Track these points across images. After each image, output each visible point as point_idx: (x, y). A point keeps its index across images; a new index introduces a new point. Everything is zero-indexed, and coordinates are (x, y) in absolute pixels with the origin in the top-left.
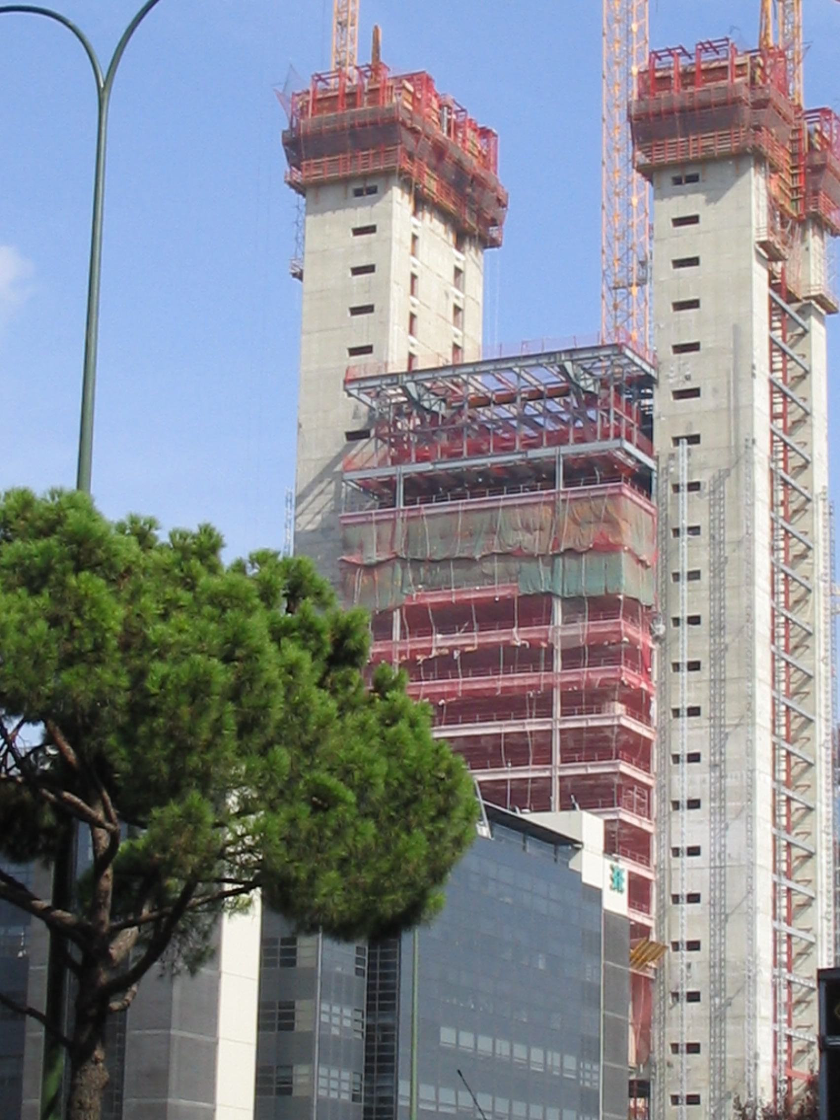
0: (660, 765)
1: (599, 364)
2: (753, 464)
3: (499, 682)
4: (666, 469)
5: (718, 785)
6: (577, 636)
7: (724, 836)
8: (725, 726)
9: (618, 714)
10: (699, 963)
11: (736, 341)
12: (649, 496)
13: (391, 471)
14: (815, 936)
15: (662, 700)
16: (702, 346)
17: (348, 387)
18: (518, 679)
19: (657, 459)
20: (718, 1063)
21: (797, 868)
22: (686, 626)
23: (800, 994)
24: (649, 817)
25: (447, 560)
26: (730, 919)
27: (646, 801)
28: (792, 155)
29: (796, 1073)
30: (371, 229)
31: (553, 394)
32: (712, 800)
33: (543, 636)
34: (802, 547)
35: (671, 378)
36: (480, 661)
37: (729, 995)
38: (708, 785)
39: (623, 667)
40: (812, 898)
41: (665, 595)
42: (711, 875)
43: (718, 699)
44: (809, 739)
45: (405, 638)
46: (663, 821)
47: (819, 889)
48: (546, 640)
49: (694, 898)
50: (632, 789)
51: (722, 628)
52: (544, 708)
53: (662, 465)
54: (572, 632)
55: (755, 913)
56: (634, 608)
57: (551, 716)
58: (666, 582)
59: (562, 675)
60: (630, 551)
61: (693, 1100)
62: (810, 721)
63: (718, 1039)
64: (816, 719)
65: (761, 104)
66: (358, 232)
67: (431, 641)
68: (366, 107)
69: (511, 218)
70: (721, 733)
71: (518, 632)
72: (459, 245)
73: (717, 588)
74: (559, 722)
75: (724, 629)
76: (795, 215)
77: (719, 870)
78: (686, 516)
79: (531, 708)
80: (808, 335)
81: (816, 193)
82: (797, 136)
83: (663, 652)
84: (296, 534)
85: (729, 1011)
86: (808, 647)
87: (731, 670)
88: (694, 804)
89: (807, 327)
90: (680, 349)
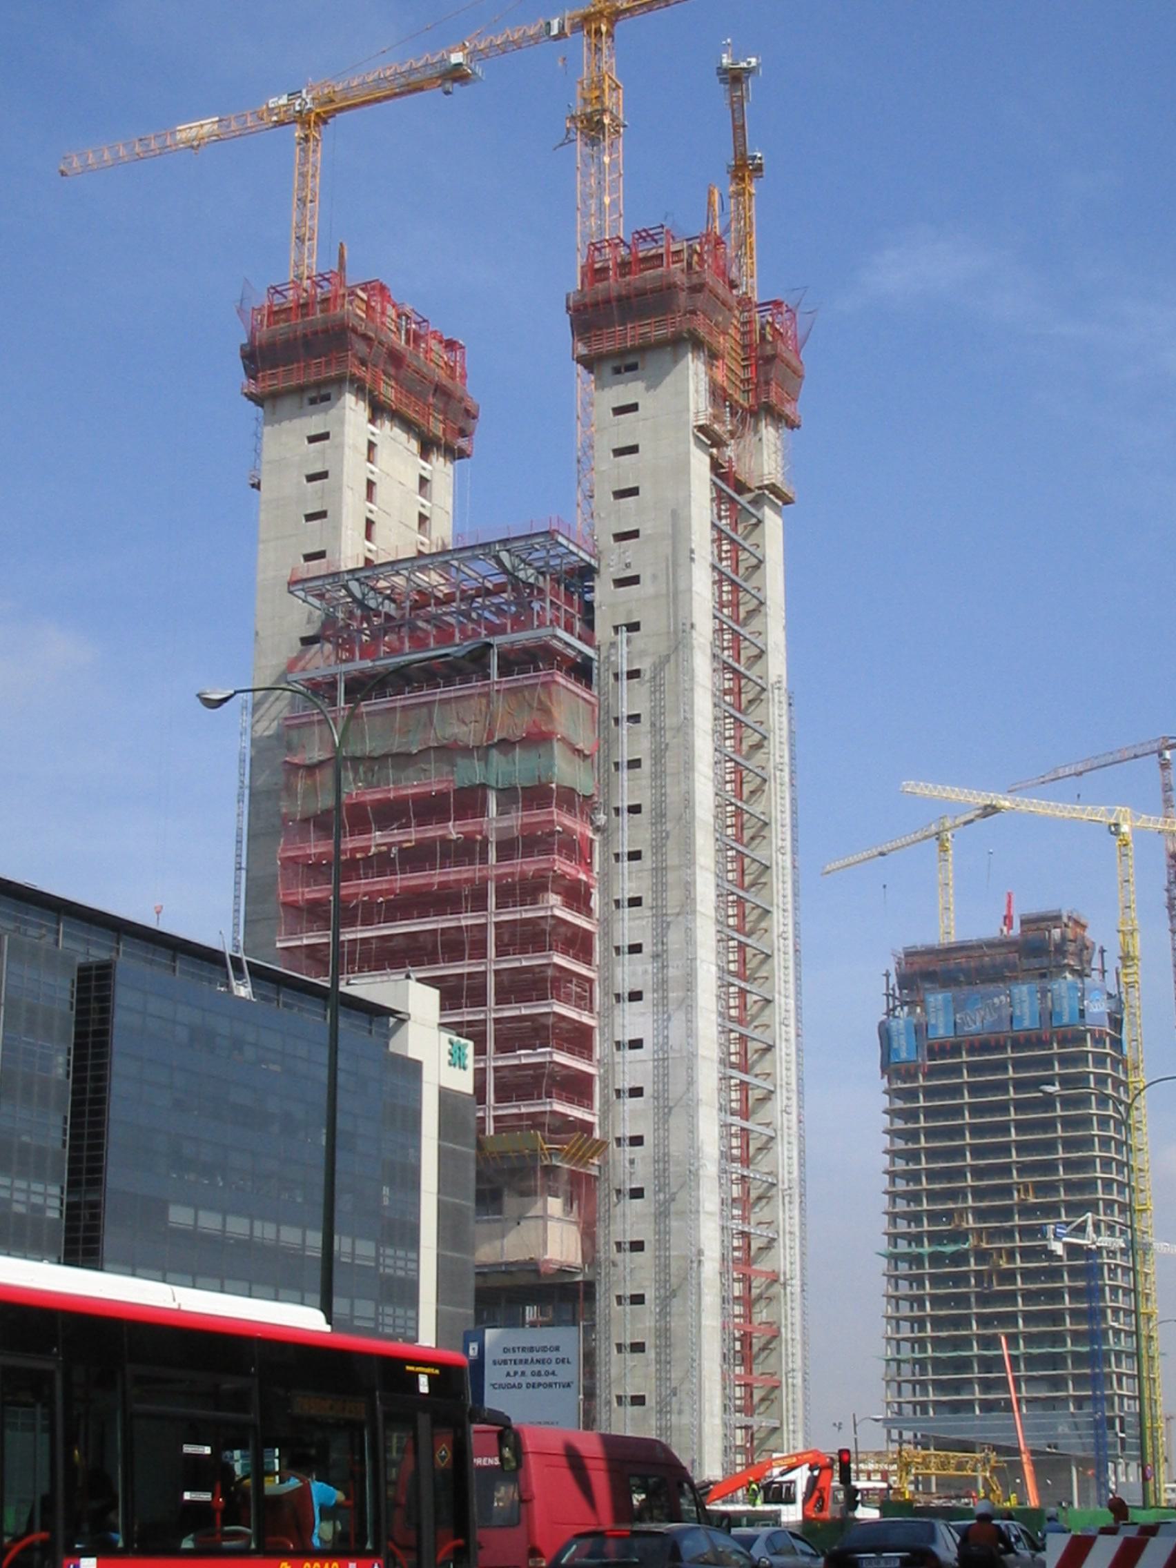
0: (602, 958)
1: (535, 555)
2: (692, 648)
3: (436, 877)
4: (608, 657)
7: (667, 1027)
8: (666, 915)
9: (554, 905)
10: (643, 1158)
11: (674, 526)
12: (589, 686)
13: (332, 670)
14: (775, 1131)
15: (605, 892)
17: (292, 589)
19: (598, 649)
21: (756, 1062)
22: (626, 814)
23: (761, 1190)
24: (591, 1010)
25: (386, 756)
26: (673, 1112)
28: (744, 347)
29: (755, 1271)
30: (324, 436)
31: (500, 589)
32: (654, 991)
33: (478, 828)
35: (610, 569)
36: (417, 857)
37: (674, 1190)
39: (556, 857)
40: (772, 1092)
41: (607, 785)
42: (654, 1067)
43: (660, 887)
44: (766, 931)
46: (607, 1015)
47: (778, 1083)
48: (480, 833)
49: (636, 1092)
50: (571, 982)
51: (663, 815)
52: (479, 902)
54: (505, 824)
55: (697, 1104)
56: (569, 799)
58: (608, 770)
59: (496, 866)
60: (563, 740)
61: (638, 1299)
62: (768, 912)
63: (663, 1236)
64: (774, 910)
65: (696, 289)
66: (313, 439)
68: (319, 315)
69: (481, 428)
72: (425, 453)
73: (658, 775)
74: (493, 916)
75: (669, 819)
76: (746, 405)
77: (662, 1063)
78: (625, 704)
81: (767, 383)
82: (747, 328)
83: (606, 843)
84: (253, 741)
85: (673, 1207)
86: (764, 837)
87: (673, 859)
88: (636, 996)
89: (760, 517)
90: (620, 537)
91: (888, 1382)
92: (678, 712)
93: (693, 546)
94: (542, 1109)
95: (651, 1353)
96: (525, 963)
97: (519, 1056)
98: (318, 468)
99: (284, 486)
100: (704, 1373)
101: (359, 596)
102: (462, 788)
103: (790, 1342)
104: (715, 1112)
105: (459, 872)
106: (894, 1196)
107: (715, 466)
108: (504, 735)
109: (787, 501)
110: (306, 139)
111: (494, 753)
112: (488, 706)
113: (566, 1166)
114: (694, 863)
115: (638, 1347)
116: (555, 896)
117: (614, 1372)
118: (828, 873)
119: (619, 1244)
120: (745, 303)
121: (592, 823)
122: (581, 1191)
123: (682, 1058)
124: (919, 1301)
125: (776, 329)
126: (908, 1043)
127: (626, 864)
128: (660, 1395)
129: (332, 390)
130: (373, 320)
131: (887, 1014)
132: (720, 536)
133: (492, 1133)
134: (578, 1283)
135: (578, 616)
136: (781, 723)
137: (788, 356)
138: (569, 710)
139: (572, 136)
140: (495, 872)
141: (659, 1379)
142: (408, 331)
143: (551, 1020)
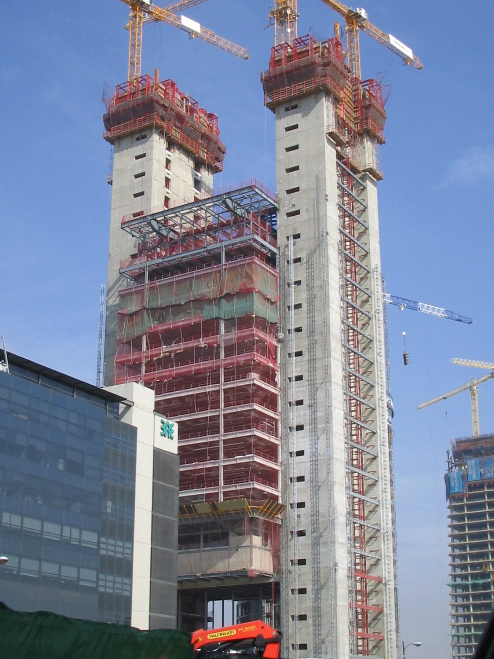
2: (327, 245)
3: (193, 367)
4: (284, 252)
5: (313, 416)
6: (232, 339)
9: (255, 378)
11: (317, 185)
14: (379, 501)
15: (284, 372)
16: (300, 189)
18: (202, 365)
19: (279, 249)
20: (316, 569)
23: (372, 534)
24: (276, 436)
25: (168, 307)
26: (321, 488)
27: (274, 427)
28: (354, 102)
30: (143, 156)
34: (366, 296)
35: (284, 208)
36: (184, 357)
37: (321, 531)
38: (308, 417)
39: (255, 353)
40: (377, 481)
41: (285, 318)
43: (312, 370)
45: (148, 349)
46: (285, 438)
47: (380, 476)
48: (216, 343)
49: (301, 479)
50: (265, 420)
51: (314, 332)
52: (216, 380)
53: (282, 251)
54: (228, 337)
57: (219, 383)
58: (285, 311)
60: (259, 292)
61: (302, 591)
63: (316, 556)
64: (376, 385)
65: (325, 65)
66: (137, 158)
67: (160, 350)
69: (226, 158)
70: (314, 388)
71: (203, 340)
73: (311, 311)
75: (317, 334)
76: (356, 130)
77: (315, 462)
79: (209, 379)
80: (366, 190)
81: (367, 119)
83: (284, 348)
84: (107, 308)
85: (321, 540)
86: (370, 348)
87: (319, 354)
88: (300, 428)
90: (289, 192)
91: (453, 646)
92: (321, 279)
93: (327, 193)
94: (248, 487)
95: (310, 620)
96: (239, 410)
97: (236, 459)
98: (140, 171)
99: (123, 181)
100: (338, 631)
101: (157, 228)
102: (207, 320)
103: (388, 615)
104: (344, 489)
105: (205, 364)
106: (454, 557)
107: (339, 156)
108: (228, 291)
109: (379, 179)
110: (135, 16)
111: (223, 301)
112: (220, 278)
113: (262, 518)
114: (330, 356)
115: (303, 618)
116: (255, 374)
117: (290, 631)
118: (420, 408)
119: (292, 561)
120: (355, 81)
121: (276, 337)
122: (272, 533)
123: (325, 459)
124: (467, 607)
125: (371, 94)
126: (459, 483)
127: (294, 358)
128: (316, 643)
129: (146, 133)
130: (168, 98)
131: (449, 470)
132: (343, 194)
133: (222, 500)
134: (271, 583)
135: (268, 233)
136: (377, 289)
137: (379, 107)
138: (262, 277)
139: (272, 22)
140: (223, 363)
141: (315, 634)
142: (187, 106)
143: (253, 440)
